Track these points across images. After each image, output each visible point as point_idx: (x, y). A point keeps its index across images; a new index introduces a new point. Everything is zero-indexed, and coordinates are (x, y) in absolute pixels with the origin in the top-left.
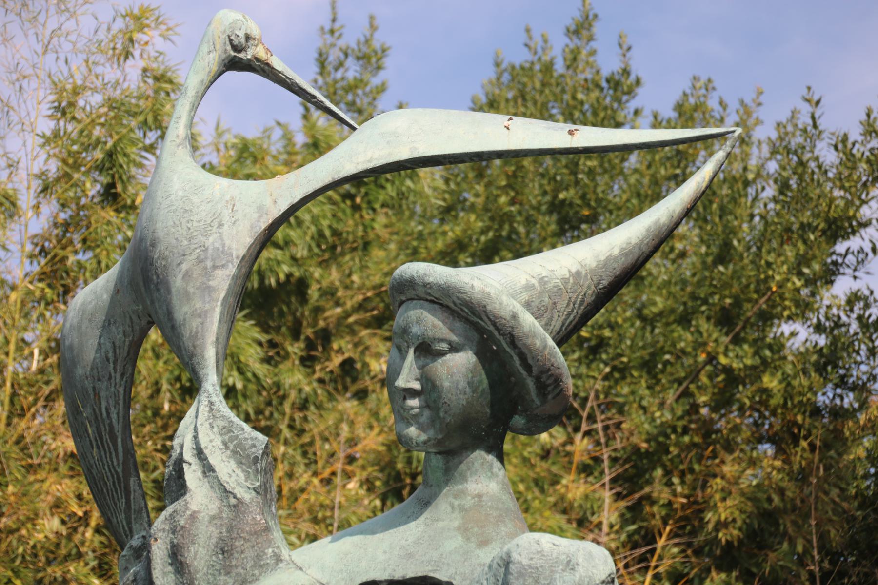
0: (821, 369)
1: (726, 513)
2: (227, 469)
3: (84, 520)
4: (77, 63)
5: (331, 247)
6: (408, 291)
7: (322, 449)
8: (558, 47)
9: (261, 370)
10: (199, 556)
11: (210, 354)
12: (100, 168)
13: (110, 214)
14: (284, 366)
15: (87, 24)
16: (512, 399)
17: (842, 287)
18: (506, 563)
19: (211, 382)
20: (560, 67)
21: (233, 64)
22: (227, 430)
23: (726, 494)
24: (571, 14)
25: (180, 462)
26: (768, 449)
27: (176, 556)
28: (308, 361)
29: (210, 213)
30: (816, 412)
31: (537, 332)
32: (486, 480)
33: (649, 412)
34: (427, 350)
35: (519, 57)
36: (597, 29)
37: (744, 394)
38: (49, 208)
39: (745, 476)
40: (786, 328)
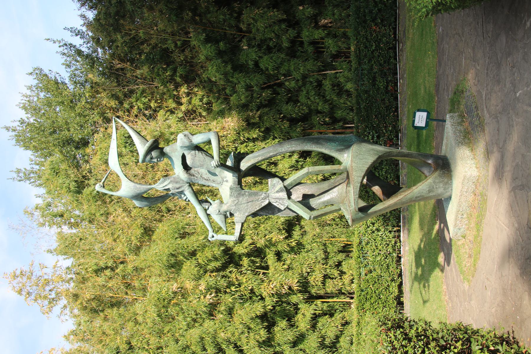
1: (113, 103)
2: (166, 183)
10: (178, 186)
14: (90, 183)
22: (160, 184)
24: (5, 131)
25: (165, 189)
27: (178, 189)
28: (89, 179)
31: (148, 144)
34: (152, 158)
35: (14, 142)
36: (7, 125)
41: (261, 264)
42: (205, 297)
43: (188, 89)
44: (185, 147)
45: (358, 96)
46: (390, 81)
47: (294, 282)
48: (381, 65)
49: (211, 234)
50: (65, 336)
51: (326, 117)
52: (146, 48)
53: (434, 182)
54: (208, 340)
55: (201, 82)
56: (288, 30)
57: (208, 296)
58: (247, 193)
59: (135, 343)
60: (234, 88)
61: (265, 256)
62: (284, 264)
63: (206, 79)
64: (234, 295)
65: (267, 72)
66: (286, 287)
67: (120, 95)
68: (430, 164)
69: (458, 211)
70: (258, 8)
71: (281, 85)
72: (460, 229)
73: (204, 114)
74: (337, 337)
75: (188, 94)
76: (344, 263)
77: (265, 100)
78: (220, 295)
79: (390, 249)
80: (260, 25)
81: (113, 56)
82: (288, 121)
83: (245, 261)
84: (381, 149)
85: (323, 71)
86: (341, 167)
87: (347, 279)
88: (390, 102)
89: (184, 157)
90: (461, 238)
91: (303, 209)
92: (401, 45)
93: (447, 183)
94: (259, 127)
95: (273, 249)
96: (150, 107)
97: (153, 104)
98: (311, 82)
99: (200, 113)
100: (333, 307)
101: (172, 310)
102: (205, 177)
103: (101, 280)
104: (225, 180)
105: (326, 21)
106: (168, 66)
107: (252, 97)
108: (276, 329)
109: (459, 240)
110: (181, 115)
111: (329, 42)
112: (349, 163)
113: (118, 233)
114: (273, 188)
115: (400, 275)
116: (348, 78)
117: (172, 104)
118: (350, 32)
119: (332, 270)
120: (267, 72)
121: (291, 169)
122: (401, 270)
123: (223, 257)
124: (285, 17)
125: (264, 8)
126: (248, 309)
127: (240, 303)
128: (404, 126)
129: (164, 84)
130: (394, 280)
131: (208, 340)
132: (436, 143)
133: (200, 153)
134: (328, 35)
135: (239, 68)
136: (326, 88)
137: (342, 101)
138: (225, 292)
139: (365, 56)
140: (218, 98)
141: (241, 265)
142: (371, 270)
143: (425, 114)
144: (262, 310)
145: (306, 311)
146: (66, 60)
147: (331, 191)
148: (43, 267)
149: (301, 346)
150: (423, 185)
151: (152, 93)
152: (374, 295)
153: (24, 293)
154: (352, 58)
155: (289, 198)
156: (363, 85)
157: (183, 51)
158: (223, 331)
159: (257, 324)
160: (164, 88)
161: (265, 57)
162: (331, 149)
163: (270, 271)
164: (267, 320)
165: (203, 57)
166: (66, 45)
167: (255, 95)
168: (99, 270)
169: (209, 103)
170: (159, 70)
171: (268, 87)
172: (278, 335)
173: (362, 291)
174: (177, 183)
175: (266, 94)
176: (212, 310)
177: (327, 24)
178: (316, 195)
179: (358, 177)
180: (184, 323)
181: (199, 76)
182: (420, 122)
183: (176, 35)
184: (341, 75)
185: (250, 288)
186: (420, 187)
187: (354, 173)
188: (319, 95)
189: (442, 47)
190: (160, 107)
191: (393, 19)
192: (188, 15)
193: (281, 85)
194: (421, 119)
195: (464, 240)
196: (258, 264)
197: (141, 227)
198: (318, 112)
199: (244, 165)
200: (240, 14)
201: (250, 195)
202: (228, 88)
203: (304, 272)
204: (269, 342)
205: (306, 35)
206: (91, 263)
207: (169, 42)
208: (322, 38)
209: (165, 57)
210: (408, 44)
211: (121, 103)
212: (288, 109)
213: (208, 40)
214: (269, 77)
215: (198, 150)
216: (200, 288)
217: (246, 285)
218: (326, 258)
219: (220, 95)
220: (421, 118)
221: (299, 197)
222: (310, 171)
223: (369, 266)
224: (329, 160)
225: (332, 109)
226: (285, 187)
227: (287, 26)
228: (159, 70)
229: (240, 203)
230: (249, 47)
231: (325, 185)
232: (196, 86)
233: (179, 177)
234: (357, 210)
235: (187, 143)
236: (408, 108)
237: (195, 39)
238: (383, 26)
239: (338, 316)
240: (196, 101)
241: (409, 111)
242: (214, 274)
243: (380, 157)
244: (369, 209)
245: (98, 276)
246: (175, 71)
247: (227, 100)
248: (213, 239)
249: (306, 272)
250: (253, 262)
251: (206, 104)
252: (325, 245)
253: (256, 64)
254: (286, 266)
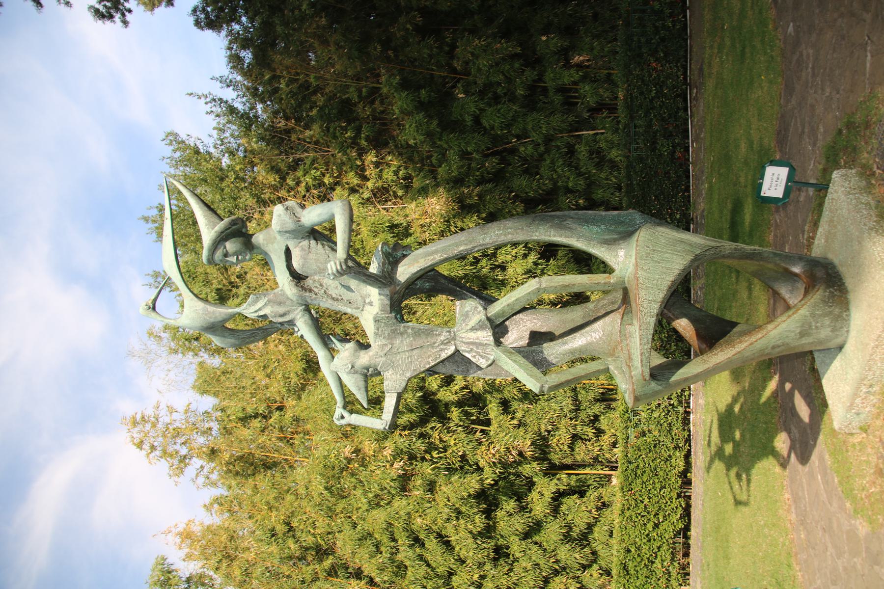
0: (234, 155)
1: (273, 179)
2: (260, 304)
3: (280, 339)
4: (163, 349)
5: (207, 283)
6: (211, 261)
7: (260, 282)
8: (151, 225)
9: (240, 299)
10: (281, 310)
11: (230, 311)
12: (190, 342)
13: (202, 339)
15: (153, 347)
16: (238, 232)
17: (212, 150)
18: (280, 232)
19: (237, 310)
20: (157, 225)
21: (154, 309)
22: (250, 305)
23: (267, 179)
24: (142, 222)
26: (255, 168)
28: (237, 287)
29: (192, 312)
30: (245, 156)
31: (220, 226)
32: (259, 239)
33: (247, 199)
34: (226, 255)
36: (146, 215)
37: (241, 175)
38: (201, 354)
39: (261, 173)
40: (224, 164)
41: (478, 418)
42: (392, 465)
43: (377, 157)
44: (286, 232)
45: (629, 166)
46: (678, 144)
47: (525, 443)
48: (663, 119)
49: (339, 411)
50: (205, 506)
51: (580, 198)
52: (320, 99)
53: (813, 315)
54: (398, 525)
55: (396, 146)
56: (524, 71)
57: (396, 465)
58: (410, 331)
59: (297, 525)
60: (444, 155)
61: (485, 406)
62: (512, 418)
63: (403, 142)
64: (437, 463)
65: (492, 132)
66: (514, 452)
67: (282, 166)
68: (796, 275)
69: (863, 380)
70: (479, 38)
71: (513, 151)
72: (858, 414)
73: (400, 193)
74: (590, 527)
75: (377, 165)
76: (602, 417)
77: (488, 173)
78: (415, 463)
79: (674, 402)
80: (483, 63)
81: (275, 113)
82: (522, 202)
83: (455, 413)
84: (696, 240)
85: (577, 131)
86: (613, 279)
87: (606, 440)
88: (677, 176)
89: (288, 253)
90: (858, 431)
91: (526, 370)
92: (695, 91)
93: (838, 318)
94: (479, 212)
95: (497, 395)
96: (324, 184)
97: (327, 180)
98: (558, 148)
99: (394, 192)
100: (584, 482)
101: (347, 482)
102: (333, 293)
103: (245, 433)
104: (367, 301)
105: (581, 58)
106: (349, 124)
107: (469, 168)
108: (500, 514)
109: (852, 434)
110: (366, 195)
111: (586, 88)
112: (631, 269)
113: (272, 366)
114: (464, 320)
115: (688, 440)
116: (613, 143)
117: (352, 179)
118: (617, 74)
119: (585, 428)
120: (492, 132)
121: (527, 276)
122: (690, 431)
123: (421, 406)
124: (518, 50)
125: (487, 37)
126: (457, 485)
127: (445, 475)
128: (699, 212)
129: (343, 148)
130: (679, 447)
131: (398, 525)
132: (775, 236)
133: (320, 246)
134: (584, 78)
135: (450, 126)
136: (581, 157)
137: (603, 176)
138: (423, 459)
139: (641, 106)
140: (421, 170)
141: (449, 419)
142: (644, 432)
143: (783, 172)
144: (477, 486)
145: (546, 488)
146: (219, 123)
147: (587, 329)
148: (171, 410)
149: (536, 538)
150: (789, 321)
151: (327, 164)
152: (647, 470)
153: (146, 447)
154: (620, 108)
155: (498, 343)
156: (636, 150)
157: (372, 102)
158: (420, 516)
159: (471, 507)
160: (343, 155)
161: (490, 110)
162: (589, 240)
163: (491, 428)
164: (487, 500)
165: (397, 111)
166: (214, 100)
167: (473, 165)
168: (246, 418)
169: (408, 178)
170: (335, 129)
171: (494, 154)
172: (502, 523)
173: (630, 462)
174: (280, 304)
175: (491, 164)
176: (404, 482)
177: (583, 61)
178: (557, 333)
179: (649, 301)
180: (365, 501)
181: (393, 138)
182: (773, 188)
183: (362, 80)
184: (602, 137)
185: (460, 453)
186: (784, 325)
187: (642, 294)
188: (569, 165)
189: (795, 58)
190: (337, 183)
191: (682, 53)
192: (375, 49)
193: (513, 151)
194: (774, 181)
195: (864, 435)
196: (474, 418)
197: (302, 359)
198: (568, 191)
199: (405, 271)
200: (453, 47)
201: (417, 334)
202: (436, 155)
203: (542, 430)
204: (488, 532)
205: (550, 80)
206: (235, 408)
207: (352, 89)
208: (575, 83)
209: (345, 111)
210: (710, 84)
211: (283, 179)
212: (521, 183)
213: (405, 85)
214: (496, 139)
215: (315, 239)
216: (385, 453)
217: (454, 449)
218: (577, 409)
219: (423, 165)
220: (775, 179)
221: (521, 338)
222: (544, 286)
223: (642, 426)
224: (584, 262)
225: (589, 186)
226: (488, 319)
227: (522, 65)
228: (335, 129)
229: (395, 350)
230: (467, 95)
231: (576, 314)
232: (389, 153)
233: (284, 294)
234: (647, 374)
235: (290, 225)
236: (710, 183)
237: (387, 82)
238: (667, 62)
239: (592, 495)
240: (388, 175)
241: (711, 188)
242: (406, 432)
243: (696, 258)
244: (673, 374)
245: (245, 426)
246: (358, 130)
247: (433, 173)
248: (343, 422)
249: (546, 431)
250: (467, 414)
251: (404, 179)
252: (575, 390)
253: (477, 120)
254: (515, 422)
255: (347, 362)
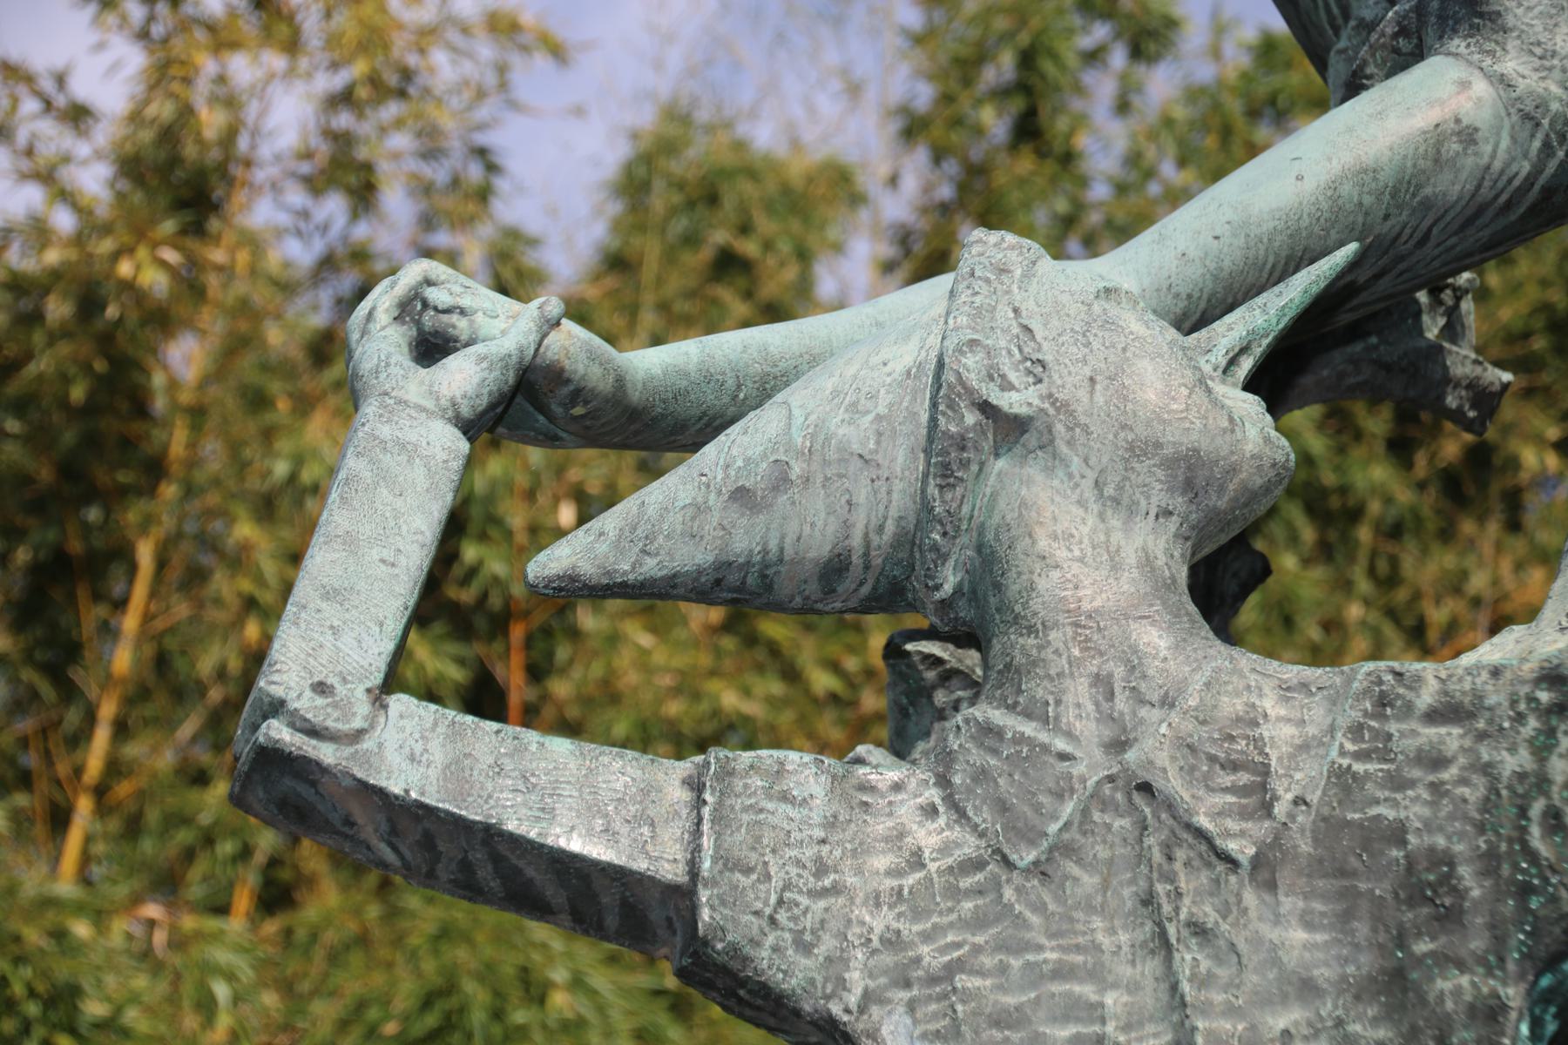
13: (1025, 164)
248: (380, 341)
255: (1068, 380)
